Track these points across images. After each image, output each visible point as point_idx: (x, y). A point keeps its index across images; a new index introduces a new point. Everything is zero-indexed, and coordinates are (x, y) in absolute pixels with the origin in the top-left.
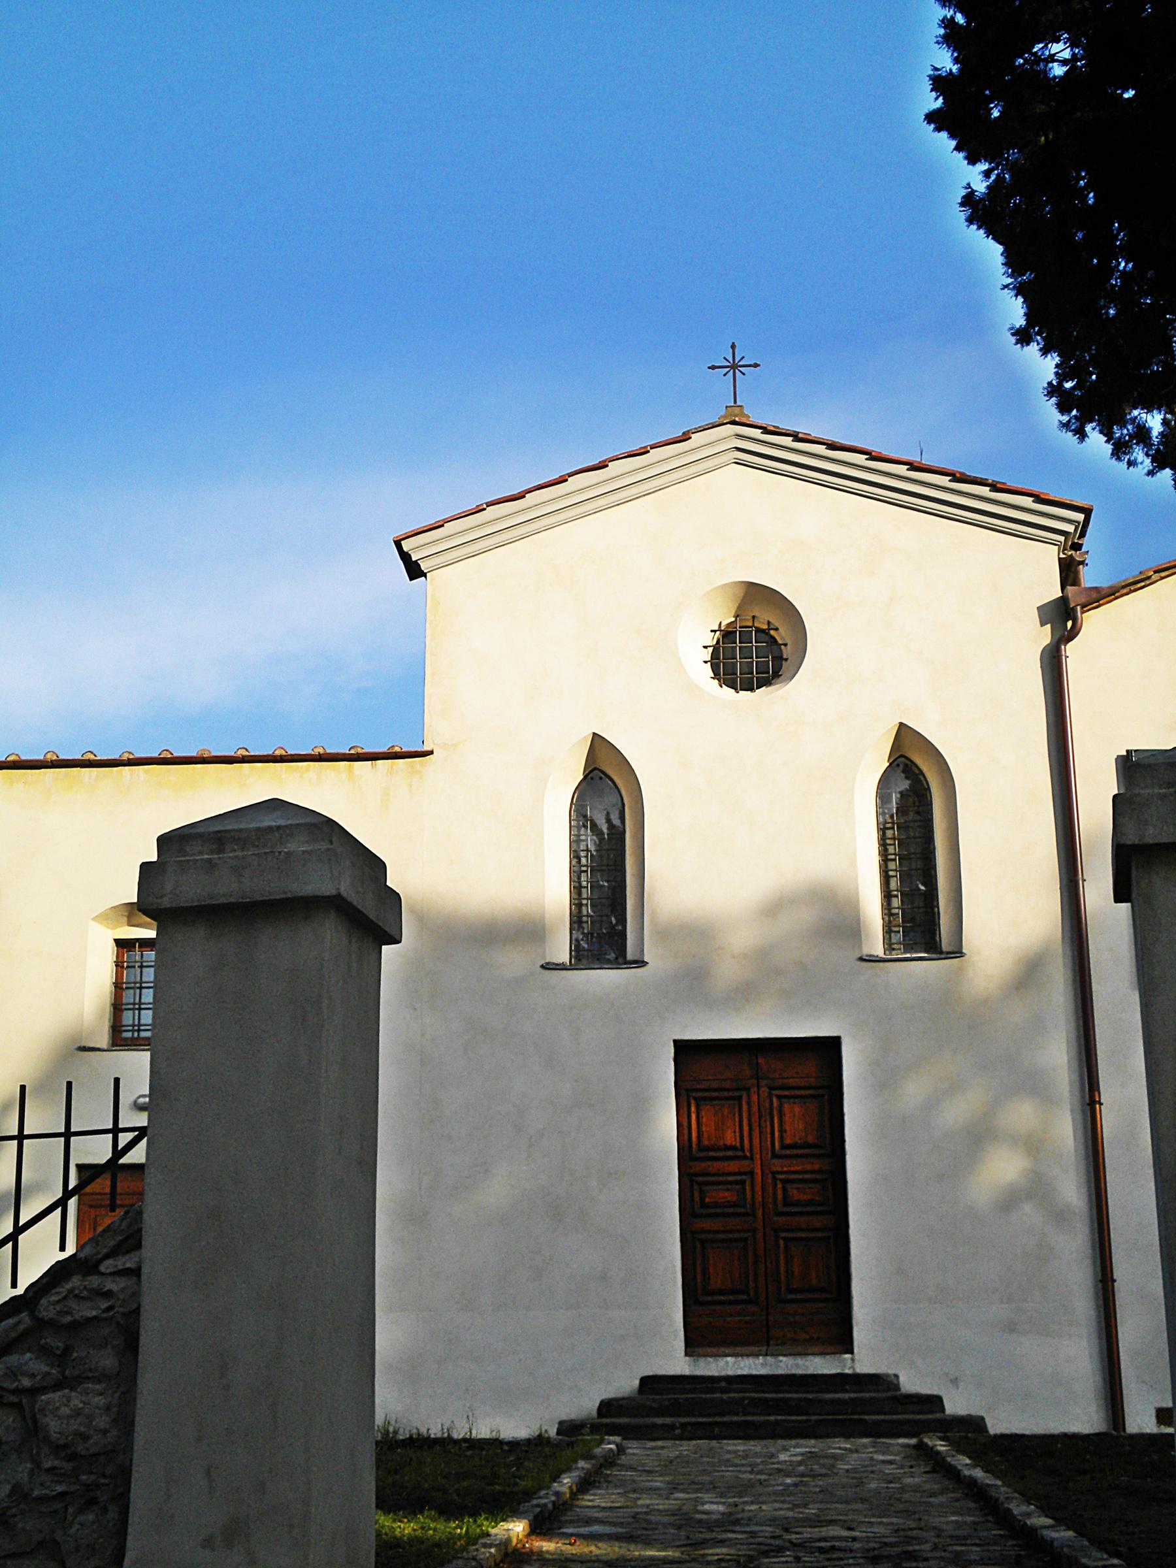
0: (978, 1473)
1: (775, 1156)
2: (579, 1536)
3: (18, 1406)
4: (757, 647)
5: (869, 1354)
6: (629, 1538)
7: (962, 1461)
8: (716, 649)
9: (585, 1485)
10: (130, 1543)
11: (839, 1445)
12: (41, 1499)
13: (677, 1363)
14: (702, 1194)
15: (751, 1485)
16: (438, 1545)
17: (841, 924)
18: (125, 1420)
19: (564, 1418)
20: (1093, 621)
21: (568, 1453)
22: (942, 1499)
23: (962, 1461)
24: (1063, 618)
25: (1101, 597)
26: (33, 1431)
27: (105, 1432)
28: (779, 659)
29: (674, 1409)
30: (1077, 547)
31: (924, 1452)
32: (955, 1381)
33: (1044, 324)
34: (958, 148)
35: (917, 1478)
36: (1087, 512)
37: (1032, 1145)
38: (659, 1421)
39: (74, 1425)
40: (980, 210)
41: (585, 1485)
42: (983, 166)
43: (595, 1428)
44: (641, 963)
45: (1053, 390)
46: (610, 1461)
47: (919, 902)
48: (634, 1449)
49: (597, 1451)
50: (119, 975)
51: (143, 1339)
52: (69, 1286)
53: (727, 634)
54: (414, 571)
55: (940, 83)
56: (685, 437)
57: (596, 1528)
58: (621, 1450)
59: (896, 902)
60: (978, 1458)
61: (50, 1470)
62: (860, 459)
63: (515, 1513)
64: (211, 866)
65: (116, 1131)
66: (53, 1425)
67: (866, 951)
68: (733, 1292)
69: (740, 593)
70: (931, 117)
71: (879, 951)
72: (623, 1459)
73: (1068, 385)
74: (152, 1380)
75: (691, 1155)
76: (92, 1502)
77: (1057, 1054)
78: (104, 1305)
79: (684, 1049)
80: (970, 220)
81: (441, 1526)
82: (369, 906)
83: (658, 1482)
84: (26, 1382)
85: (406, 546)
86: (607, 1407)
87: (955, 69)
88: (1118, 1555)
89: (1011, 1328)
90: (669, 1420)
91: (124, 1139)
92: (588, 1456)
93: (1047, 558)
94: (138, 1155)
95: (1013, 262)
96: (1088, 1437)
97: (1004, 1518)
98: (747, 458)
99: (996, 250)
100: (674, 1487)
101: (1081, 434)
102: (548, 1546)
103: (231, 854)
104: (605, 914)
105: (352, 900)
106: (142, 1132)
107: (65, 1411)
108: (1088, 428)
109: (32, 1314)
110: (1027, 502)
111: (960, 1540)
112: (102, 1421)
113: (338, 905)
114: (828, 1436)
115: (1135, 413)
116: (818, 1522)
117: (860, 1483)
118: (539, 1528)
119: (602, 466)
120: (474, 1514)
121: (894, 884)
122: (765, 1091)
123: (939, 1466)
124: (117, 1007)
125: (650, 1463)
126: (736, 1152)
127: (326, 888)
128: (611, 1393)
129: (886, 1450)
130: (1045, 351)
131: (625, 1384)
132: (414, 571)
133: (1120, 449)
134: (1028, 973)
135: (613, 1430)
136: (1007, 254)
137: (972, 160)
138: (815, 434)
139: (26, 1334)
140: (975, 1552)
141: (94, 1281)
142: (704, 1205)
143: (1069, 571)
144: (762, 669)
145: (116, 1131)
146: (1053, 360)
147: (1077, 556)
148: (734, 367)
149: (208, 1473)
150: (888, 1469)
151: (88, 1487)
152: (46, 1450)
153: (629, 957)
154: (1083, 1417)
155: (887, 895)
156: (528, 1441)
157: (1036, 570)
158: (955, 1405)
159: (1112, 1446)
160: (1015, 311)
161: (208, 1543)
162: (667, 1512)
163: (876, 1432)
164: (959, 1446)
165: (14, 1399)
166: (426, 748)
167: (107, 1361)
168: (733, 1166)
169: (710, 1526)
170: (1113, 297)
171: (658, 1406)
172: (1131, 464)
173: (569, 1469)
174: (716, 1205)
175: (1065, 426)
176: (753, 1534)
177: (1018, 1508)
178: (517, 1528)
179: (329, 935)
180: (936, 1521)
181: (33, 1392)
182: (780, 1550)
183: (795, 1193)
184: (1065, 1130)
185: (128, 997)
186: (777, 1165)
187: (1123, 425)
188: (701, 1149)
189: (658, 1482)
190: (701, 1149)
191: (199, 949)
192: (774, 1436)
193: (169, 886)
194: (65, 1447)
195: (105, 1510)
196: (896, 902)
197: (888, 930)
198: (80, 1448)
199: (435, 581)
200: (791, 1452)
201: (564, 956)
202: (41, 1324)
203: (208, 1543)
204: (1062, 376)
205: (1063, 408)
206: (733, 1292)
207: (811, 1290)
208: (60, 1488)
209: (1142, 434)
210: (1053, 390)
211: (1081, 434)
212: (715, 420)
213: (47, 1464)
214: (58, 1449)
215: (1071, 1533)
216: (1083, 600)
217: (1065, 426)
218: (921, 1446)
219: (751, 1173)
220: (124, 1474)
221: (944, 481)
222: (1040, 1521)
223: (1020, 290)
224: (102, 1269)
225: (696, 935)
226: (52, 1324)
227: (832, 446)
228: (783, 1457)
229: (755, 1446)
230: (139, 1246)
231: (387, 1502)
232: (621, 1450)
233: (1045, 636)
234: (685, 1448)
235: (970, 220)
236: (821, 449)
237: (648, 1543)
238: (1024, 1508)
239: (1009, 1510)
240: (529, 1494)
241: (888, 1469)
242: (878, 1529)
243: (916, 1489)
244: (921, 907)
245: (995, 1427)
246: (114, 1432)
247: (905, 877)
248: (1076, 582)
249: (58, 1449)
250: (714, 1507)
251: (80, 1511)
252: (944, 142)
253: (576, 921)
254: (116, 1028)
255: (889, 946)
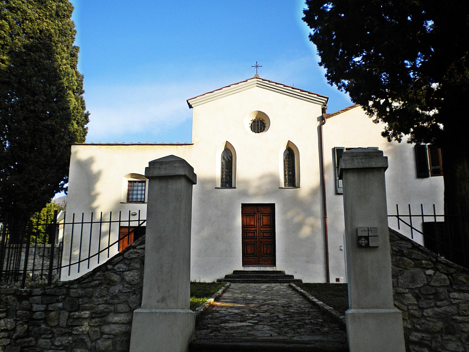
0: (302, 291)
1: (261, 227)
2: (224, 302)
3: (120, 274)
4: (260, 124)
5: (279, 267)
6: (234, 302)
7: (298, 288)
8: (252, 124)
9: (224, 292)
10: (142, 302)
11: (273, 285)
12: (125, 293)
13: (240, 267)
14: (246, 235)
15: (257, 292)
16: (197, 303)
17: (275, 181)
18: (141, 278)
19: (218, 278)
20: (328, 121)
21: (220, 286)
22: (295, 295)
23: (298, 288)
24: (322, 120)
25: (330, 116)
26: (123, 279)
27: (137, 280)
28: (264, 127)
29: (240, 277)
30: (325, 105)
31: (290, 286)
32: (296, 273)
33: (325, 62)
34: (308, 25)
35: (290, 291)
36: (328, 98)
37: (312, 226)
38: (237, 279)
39: (131, 278)
40: (312, 38)
41: (224, 292)
42: (313, 29)
43: (224, 281)
44: (235, 188)
45: (326, 75)
46: (228, 287)
47: (291, 177)
48: (233, 285)
49: (226, 285)
50: (129, 188)
51: (145, 262)
52: (130, 251)
53: (254, 121)
54: (190, 107)
55: (305, 12)
56: (247, 81)
57: (227, 300)
58: (230, 285)
59: (287, 177)
60: (302, 288)
61: (126, 287)
62: (282, 86)
63: (211, 297)
64: (160, 168)
65: (139, 220)
66: (127, 278)
67: (281, 186)
68: (252, 254)
69: (257, 113)
70: (303, 19)
71: (283, 187)
72: (230, 287)
73: (329, 74)
74: (147, 269)
75: (244, 227)
76: (135, 293)
77: (318, 208)
78: (137, 255)
79: (243, 205)
80: (310, 40)
81: (196, 299)
82: (191, 177)
83: (238, 291)
84: (121, 270)
85: (189, 102)
86: (226, 277)
87: (308, 9)
88: (331, 307)
89: (308, 262)
90: (239, 279)
91: (141, 222)
92: (224, 286)
93: (319, 107)
94: (144, 224)
95: (319, 49)
96: (323, 284)
97: (308, 300)
98: (259, 85)
99: (315, 46)
100: (241, 293)
101: (332, 85)
102: (218, 304)
103: (164, 166)
104: (228, 178)
105: (190, 177)
106: (145, 221)
107: (129, 275)
108: (333, 83)
109: (123, 257)
110: (316, 96)
111: (299, 303)
112: (137, 278)
113: (185, 176)
114: (272, 283)
115: (343, 80)
116: (271, 300)
117: (278, 292)
118: (216, 300)
119: (229, 86)
120: (203, 297)
121: (286, 173)
122: (259, 214)
123: (294, 289)
124: (128, 194)
125: (236, 288)
126: (253, 226)
127: (183, 173)
128: (227, 274)
129: (283, 286)
130: (325, 67)
131: (230, 272)
132: (190, 107)
133: (339, 88)
134: (313, 193)
135: (228, 281)
136: (318, 47)
137: (311, 28)
138: (273, 81)
139: (121, 260)
140: (303, 306)
141: (135, 250)
142: (247, 237)
143: (324, 110)
144: (261, 128)
145: (139, 220)
146: (326, 69)
147: (325, 107)
148: (257, 66)
149: (158, 288)
150: (284, 290)
151: (134, 290)
152: (125, 283)
153: (233, 186)
154: (321, 280)
155: (285, 175)
156: (211, 283)
157: (317, 110)
158: (296, 277)
159: (327, 286)
160: (319, 59)
161: (158, 302)
162: (241, 297)
163: (280, 282)
164: (298, 285)
165: (119, 273)
166: (192, 143)
167: (138, 266)
168: (253, 229)
169: (250, 300)
170: (338, 57)
171: (237, 276)
172: (342, 91)
173: (220, 289)
174: (248, 237)
175: (329, 83)
176: (258, 302)
177: (311, 297)
178: (212, 300)
179: (182, 183)
180: (294, 300)
181: (123, 272)
182: (264, 305)
183: (265, 235)
184: (319, 223)
185: (131, 192)
186: (262, 229)
187: (340, 83)
188: (246, 225)
189: (238, 291)
190: (246, 225)
191: (157, 185)
192: (260, 283)
193: (151, 172)
194: (129, 282)
195: (137, 295)
196: (287, 177)
197: (285, 182)
198: (132, 283)
199: (195, 109)
200: (264, 286)
201: (220, 186)
202: (124, 258)
203: (158, 302)
204: (328, 73)
205: (328, 79)
206: (252, 254)
207: (268, 254)
208: (128, 291)
209: (344, 85)
210: (326, 75)
211: (332, 85)
212: (253, 77)
213: (126, 286)
214: (128, 283)
215: (322, 303)
216: (326, 116)
217: (329, 83)
218: (290, 285)
219: (256, 230)
220: (141, 288)
221: (299, 91)
222: (315, 300)
223: (320, 55)
224: (137, 248)
225: (246, 182)
226: (127, 258)
227: (276, 83)
228: (262, 287)
229: (256, 285)
230: (144, 243)
231: (192, 295)
232: (230, 285)
233: (318, 123)
234: (243, 285)
235: (310, 40)
236: (274, 84)
237: (238, 303)
238: (312, 297)
239: (309, 298)
240: (213, 294)
241: (284, 290)
242: (283, 301)
243: (290, 294)
244: (292, 178)
245: (304, 282)
246: (139, 280)
247: (289, 172)
248: (325, 113)
249: (128, 283)
250: (250, 297)
251: (133, 295)
252: (306, 24)
253: (222, 179)
254: (128, 199)
255: (285, 185)
